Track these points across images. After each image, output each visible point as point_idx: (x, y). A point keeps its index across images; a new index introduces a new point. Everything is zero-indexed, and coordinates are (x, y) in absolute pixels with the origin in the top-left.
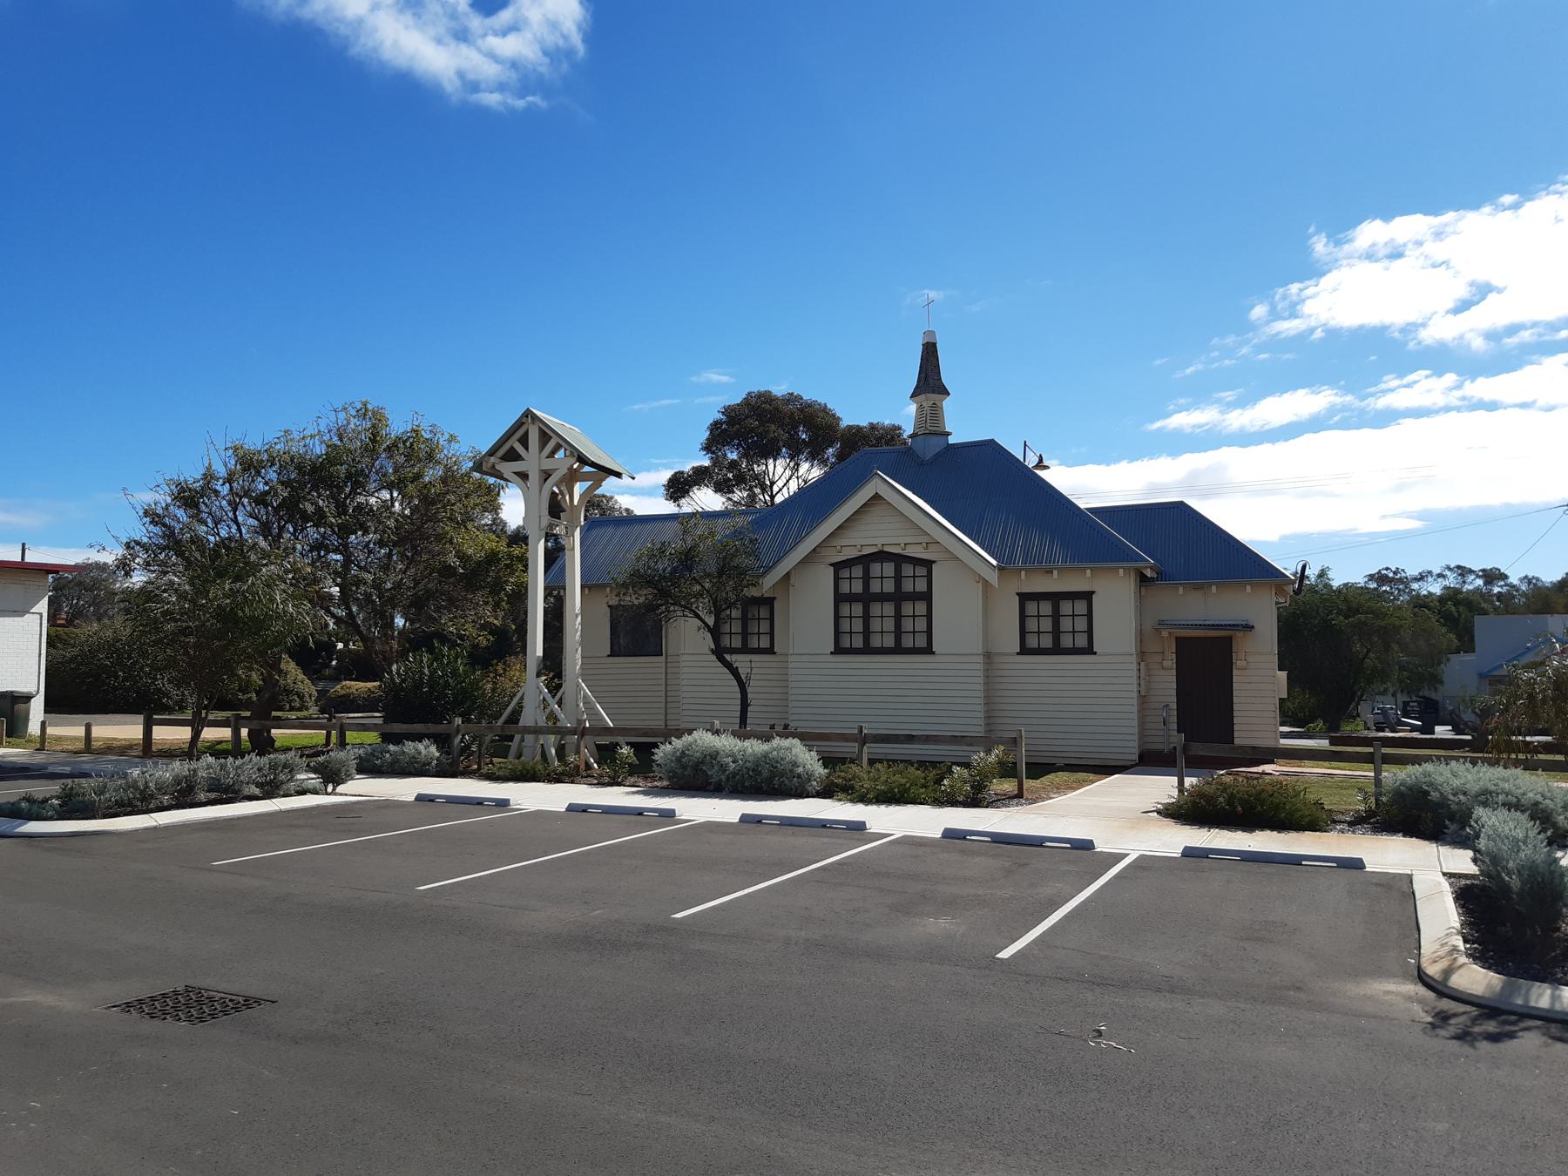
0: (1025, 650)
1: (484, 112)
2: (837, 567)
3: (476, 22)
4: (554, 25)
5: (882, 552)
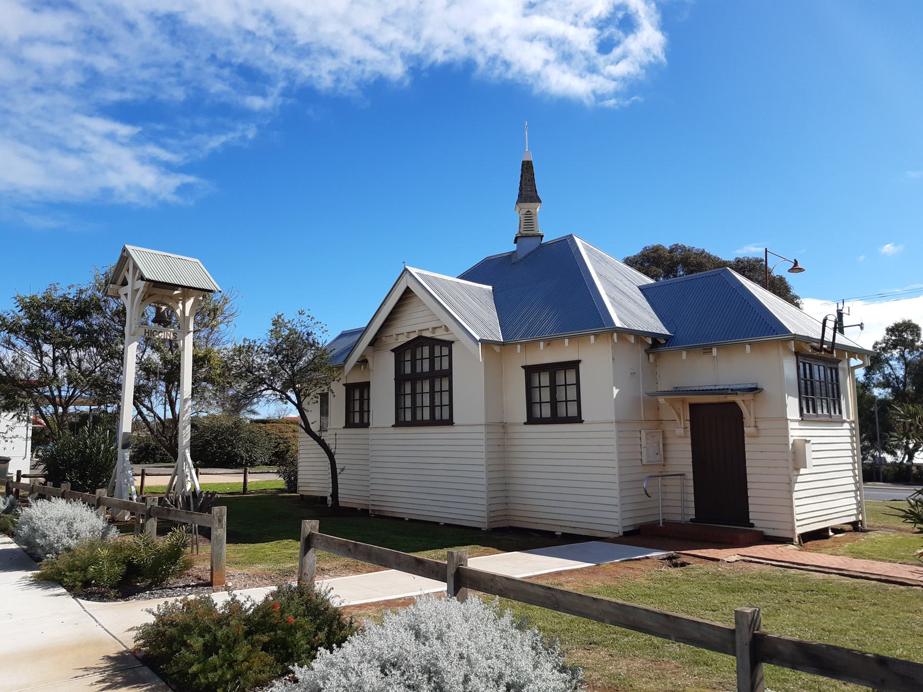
0: (532, 420)
1: (606, 111)
2: (399, 352)
3: (601, 59)
4: (648, 51)
5: (420, 338)
